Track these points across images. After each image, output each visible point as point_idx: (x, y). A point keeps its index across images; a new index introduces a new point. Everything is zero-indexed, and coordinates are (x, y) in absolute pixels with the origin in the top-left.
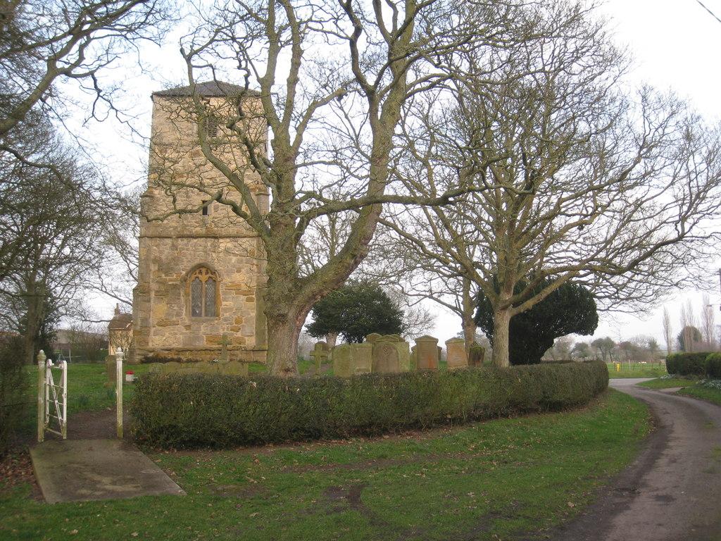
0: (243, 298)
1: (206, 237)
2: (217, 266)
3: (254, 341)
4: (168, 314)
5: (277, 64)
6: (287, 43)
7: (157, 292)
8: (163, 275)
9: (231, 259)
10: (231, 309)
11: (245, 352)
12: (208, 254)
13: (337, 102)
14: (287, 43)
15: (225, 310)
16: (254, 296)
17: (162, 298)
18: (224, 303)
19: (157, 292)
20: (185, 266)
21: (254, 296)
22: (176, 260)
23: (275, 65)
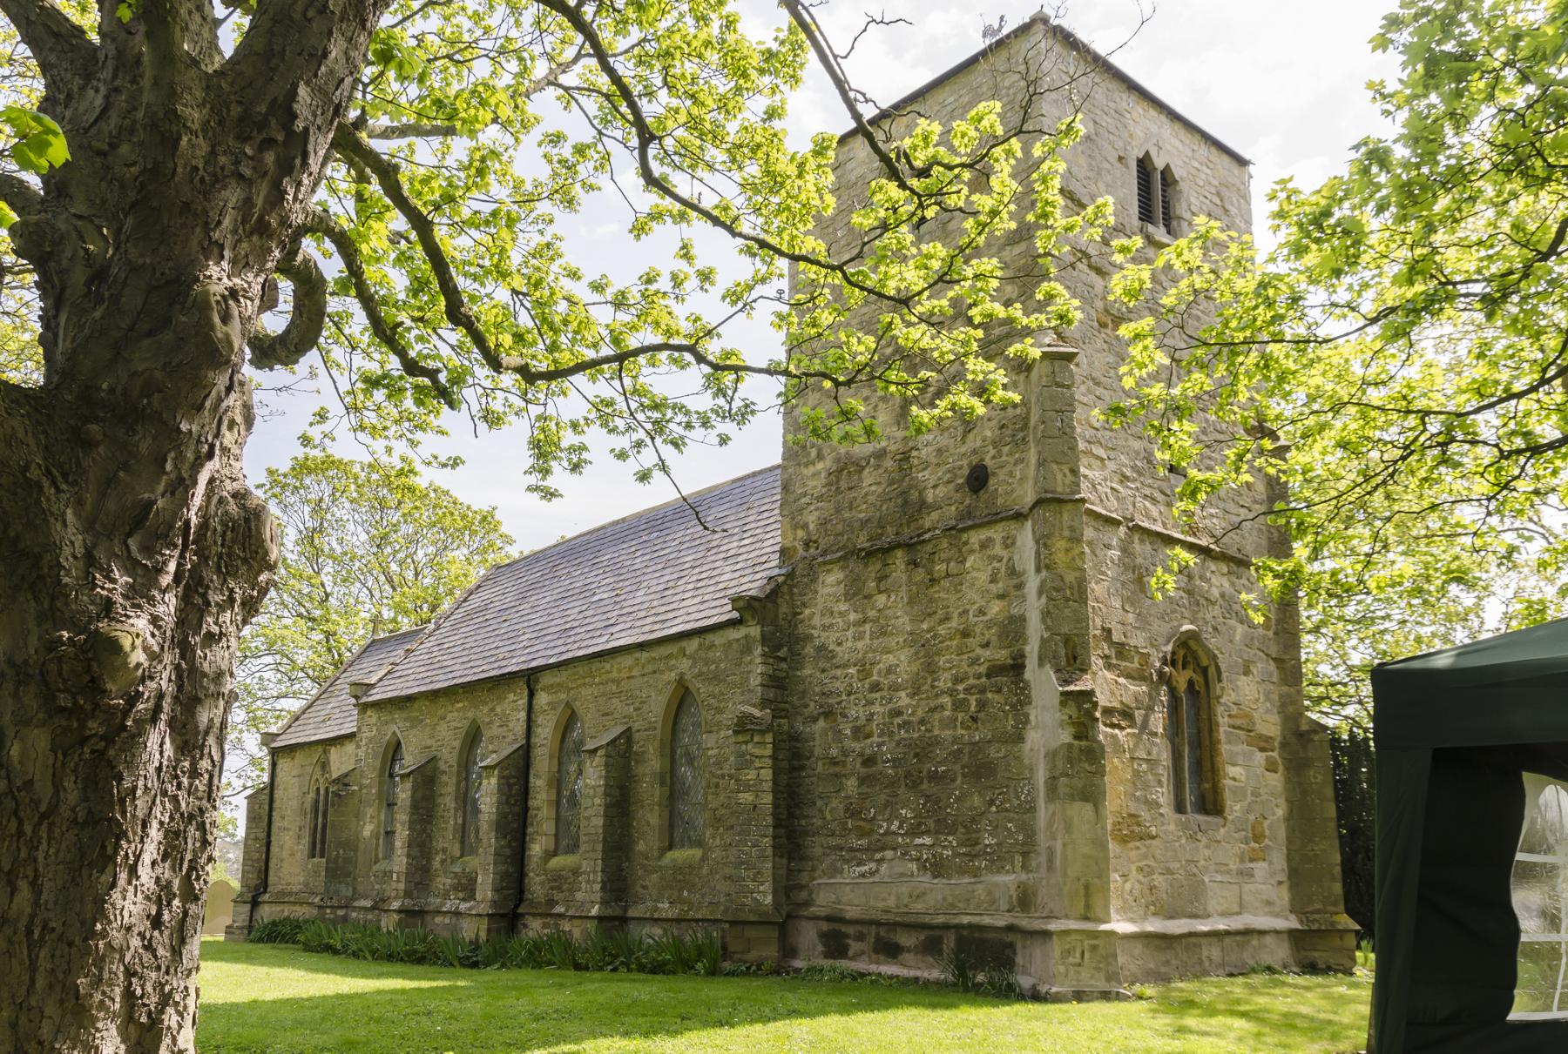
0: (1260, 757)
18: (1232, 771)
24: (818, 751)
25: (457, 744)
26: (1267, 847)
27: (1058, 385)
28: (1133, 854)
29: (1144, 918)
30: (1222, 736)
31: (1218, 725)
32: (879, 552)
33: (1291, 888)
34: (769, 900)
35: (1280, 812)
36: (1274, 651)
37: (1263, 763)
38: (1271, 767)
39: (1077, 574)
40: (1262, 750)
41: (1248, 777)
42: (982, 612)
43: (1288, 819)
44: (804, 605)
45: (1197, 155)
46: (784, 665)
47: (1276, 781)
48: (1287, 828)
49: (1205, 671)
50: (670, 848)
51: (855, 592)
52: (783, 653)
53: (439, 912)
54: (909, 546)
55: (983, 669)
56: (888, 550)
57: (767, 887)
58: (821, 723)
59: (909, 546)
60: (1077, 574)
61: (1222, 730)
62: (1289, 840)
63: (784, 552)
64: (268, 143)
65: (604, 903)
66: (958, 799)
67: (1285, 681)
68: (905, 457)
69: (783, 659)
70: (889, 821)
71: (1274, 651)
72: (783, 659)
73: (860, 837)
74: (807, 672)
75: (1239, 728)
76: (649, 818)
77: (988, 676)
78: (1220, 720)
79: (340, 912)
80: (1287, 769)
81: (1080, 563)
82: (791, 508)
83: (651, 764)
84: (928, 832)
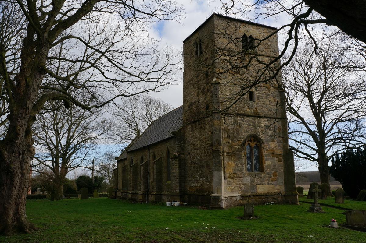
0: (276, 159)
1: (255, 116)
2: (261, 136)
3: (283, 188)
4: (235, 170)
5: (183, 89)
6: (67, 16)
7: (227, 153)
8: (230, 141)
9: (269, 132)
10: (270, 167)
11: (281, 196)
12: (256, 128)
13: (342, 151)
14: (67, 16)
15: (267, 167)
16: (282, 158)
17: (231, 158)
18: (267, 162)
19: (227, 153)
20: (243, 135)
21: (282, 158)
22: (237, 131)
23: (183, 94)
24: (188, 161)
25: (140, 160)
26: (277, 178)
27: (216, 89)
28: (235, 181)
29: (233, 192)
30: (264, 155)
31: (263, 153)
32: (194, 122)
33: (285, 186)
34: (178, 191)
35: (282, 170)
36: (281, 135)
37: (277, 160)
38: (280, 160)
39: (219, 127)
40: (277, 157)
41: (272, 164)
42: (208, 134)
43: (284, 171)
44: (186, 132)
45: (260, 31)
46: (183, 145)
47: (281, 164)
48: (284, 173)
49: (259, 142)
50: (168, 181)
51: (192, 130)
52: (182, 142)
53: (138, 194)
54: (198, 121)
55: (208, 146)
56: (196, 121)
57: (178, 188)
58: (188, 156)
59: (198, 121)
60: (219, 127)
61: (264, 154)
62: (285, 176)
63: (184, 121)
64: (24, 109)
65: (157, 192)
66: (205, 171)
67: (284, 142)
68: (198, 102)
69: (183, 143)
70: (197, 175)
71: (281, 135)
72: (183, 143)
73: (194, 178)
74: (186, 146)
75: (270, 153)
76: (165, 175)
77: (209, 147)
78: (264, 152)
79: (125, 194)
80: (284, 161)
81: (219, 125)
82: (184, 113)
83: (164, 165)
84: (202, 177)
